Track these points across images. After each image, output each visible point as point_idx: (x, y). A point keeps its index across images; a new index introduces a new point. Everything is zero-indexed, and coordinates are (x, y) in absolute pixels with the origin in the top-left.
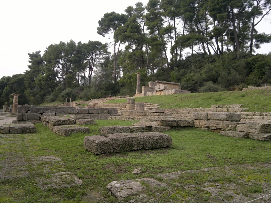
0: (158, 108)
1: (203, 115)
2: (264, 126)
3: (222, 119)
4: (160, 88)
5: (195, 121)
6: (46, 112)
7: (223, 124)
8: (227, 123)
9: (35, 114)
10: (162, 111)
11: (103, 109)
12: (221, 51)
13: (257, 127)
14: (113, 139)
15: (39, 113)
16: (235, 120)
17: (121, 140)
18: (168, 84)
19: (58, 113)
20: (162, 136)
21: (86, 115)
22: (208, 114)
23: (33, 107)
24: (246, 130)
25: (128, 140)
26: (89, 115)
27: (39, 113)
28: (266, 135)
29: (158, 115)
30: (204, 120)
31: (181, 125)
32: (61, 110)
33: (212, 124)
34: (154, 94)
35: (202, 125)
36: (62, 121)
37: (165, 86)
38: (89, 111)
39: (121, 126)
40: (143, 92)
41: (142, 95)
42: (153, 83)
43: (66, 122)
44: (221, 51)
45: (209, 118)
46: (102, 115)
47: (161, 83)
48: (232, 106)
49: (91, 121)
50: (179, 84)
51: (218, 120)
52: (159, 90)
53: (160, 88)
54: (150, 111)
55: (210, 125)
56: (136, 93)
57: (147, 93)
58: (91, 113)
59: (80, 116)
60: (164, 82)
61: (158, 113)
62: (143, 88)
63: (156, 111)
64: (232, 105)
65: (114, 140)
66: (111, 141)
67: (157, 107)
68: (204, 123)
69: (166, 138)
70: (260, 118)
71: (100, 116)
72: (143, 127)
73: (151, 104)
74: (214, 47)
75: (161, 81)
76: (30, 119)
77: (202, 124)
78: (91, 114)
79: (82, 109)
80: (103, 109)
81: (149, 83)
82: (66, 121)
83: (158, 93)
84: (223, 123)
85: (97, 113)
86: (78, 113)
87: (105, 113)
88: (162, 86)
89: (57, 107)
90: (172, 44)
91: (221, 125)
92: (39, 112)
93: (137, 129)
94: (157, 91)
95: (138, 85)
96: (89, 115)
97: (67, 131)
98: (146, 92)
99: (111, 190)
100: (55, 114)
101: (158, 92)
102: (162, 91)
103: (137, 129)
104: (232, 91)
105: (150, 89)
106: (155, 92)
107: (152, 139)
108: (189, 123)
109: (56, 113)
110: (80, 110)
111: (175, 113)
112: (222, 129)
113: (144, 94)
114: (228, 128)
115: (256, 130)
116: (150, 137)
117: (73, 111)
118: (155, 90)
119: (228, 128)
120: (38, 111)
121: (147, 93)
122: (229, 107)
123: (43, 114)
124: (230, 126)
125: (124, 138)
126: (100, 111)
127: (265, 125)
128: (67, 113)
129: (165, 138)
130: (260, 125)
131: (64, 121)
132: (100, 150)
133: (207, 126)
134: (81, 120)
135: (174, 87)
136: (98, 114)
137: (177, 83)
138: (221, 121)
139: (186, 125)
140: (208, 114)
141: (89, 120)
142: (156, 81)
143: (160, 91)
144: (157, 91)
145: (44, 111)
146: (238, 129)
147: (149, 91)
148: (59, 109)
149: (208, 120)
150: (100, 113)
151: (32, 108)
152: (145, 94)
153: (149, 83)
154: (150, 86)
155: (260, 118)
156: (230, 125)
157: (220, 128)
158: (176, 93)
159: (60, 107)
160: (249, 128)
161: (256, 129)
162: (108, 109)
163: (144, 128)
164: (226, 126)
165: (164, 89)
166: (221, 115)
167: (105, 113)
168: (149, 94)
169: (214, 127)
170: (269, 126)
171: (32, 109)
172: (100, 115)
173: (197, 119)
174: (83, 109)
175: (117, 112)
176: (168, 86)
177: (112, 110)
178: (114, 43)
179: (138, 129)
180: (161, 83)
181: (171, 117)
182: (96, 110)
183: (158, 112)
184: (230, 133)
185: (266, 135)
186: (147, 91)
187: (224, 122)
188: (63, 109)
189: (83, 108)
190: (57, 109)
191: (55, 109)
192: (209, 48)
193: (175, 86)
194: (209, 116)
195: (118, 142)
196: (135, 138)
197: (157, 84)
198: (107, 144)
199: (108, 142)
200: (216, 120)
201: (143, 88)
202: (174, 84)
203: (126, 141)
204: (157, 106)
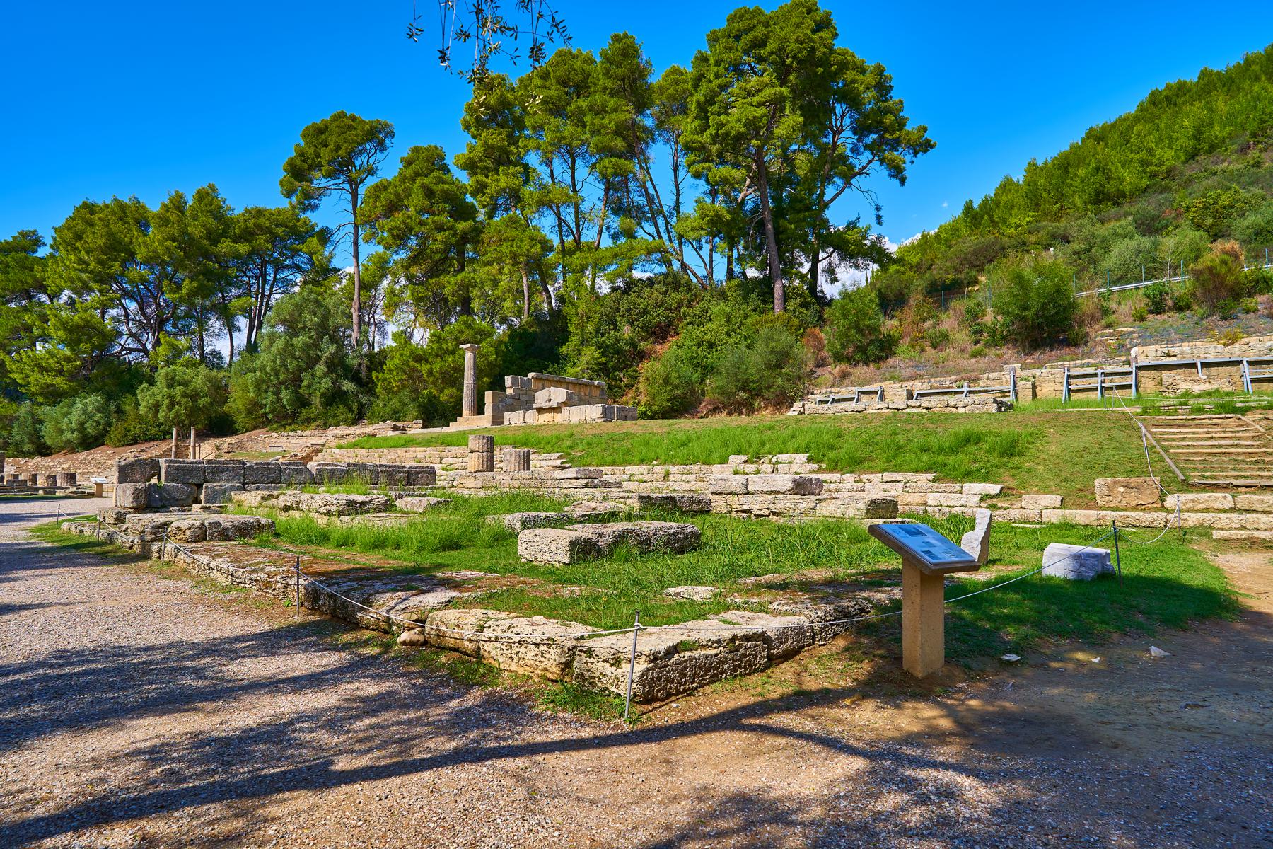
1: (735, 483)
4: (550, 400)
10: (592, 475)
12: (1167, 654)
29: (586, 486)
34: (532, 418)
40: (489, 409)
44: (1167, 654)
45: (750, 488)
48: (783, 457)
51: (772, 492)
52: (548, 405)
53: (552, 398)
55: (754, 507)
56: (461, 415)
57: (507, 415)
61: (585, 481)
63: (577, 472)
83: (546, 418)
91: (780, 506)
94: (540, 410)
115: (859, 513)
118: (534, 406)
121: (507, 415)
122: (778, 463)
124: (803, 505)
130: (866, 501)
133: (745, 507)
144: (540, 410)
154: (510, 392)
165: (565, 404)
168: (513, 418)
173: (721, 493)
178: (351, 228)
187: (789, 497)
190: (249, 468)
200: (766, 492)
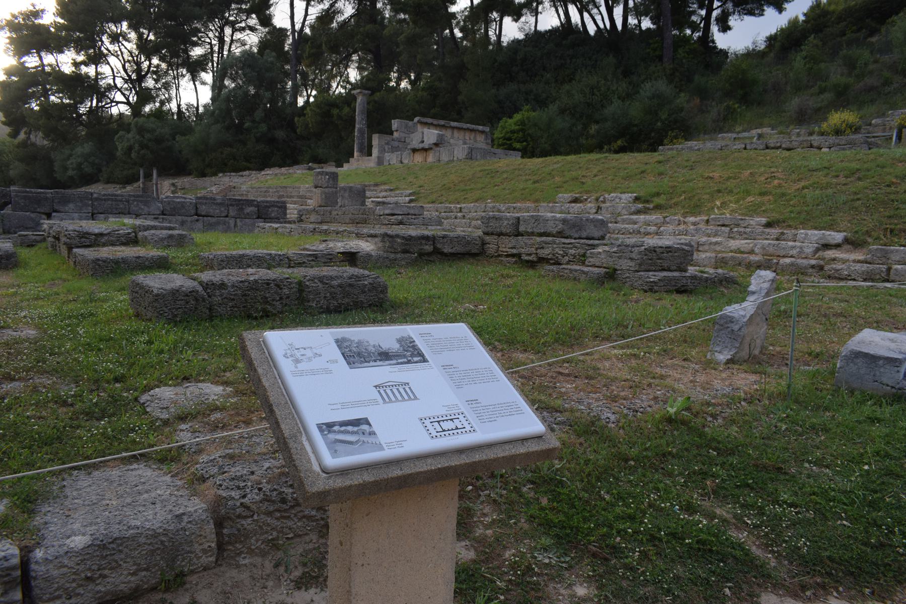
0: (411, 201)
2: (655, 251)
3: (554, 231)
5: (487, 238)
6: (62, 210)
7: (555, 246)
8: (564, 243)
9: (28, 213)
10: (412, 212)
11: (242, 202)
13: (634, 256)
14: (207, 284)
15: (39, 213)
16: (591, 235)
17: (233, 286)
18: (453, 128)
19: (100, 211)
20: (358, 278)
21: (189, 219)
22: (521, 218)
23: (19, 192)
24: (610, 262)
25: (254, 286)
26: (197, 220)
27: (39, 213)
28: (654, 276)
30: (510, 236)
31: (445, 251)
32: (109, 202)
33: (526, 246)
35: (504, 250)
36: (95, 235)
37: (439, 136)
38: (197, 208)
39: (260, 251)
40: (375, 152)
41: (370, 163)
42: (406, 126)
43: (106, 238)
45: (522, 228)
46: (238, 220)
47: (432, 124)
49: (179, 235)
50: (487, 129)
53: (425, 139)
54: (379, 210)
57: (387, 156)
58: (203, 213)
59: (170, 222)
60: (442, 122)
61: (400, 217)
62: (376, 140)
64: (612, 195)
65: (206, 286)
66: (200, 289)
67: (407, 199)
68: (507, 245)
69: (370, 284)
70: (677, 232)
71: (232, 225)
72: (331, 254)
73: (391, 190)
74: (598, 18)
75: (429, 120)
76: (12, 231)
77: (503, 246)
78: (204, 216)
79: (174, 201)
80: (242, 202)
81: (395, 124)
82: (106, 235)
84: (555, 243)
85: (224, 215)
86: (165, 215)
87: (248, 214)
88: (430, 135)
89: (95, 195)
90: (308, 18)
92: (38, 210)
93: (310, 259)
94: (414, 151)
95: (360, 130)
96: (197, 220)
97: (100, 262)
98: (382, 151)
99: (274, 440)
100: (92, 215)
101: (419, 153)
102: (431, 149)
103: (310, 259)
104: (544, 154)
105: (396, 144)
106: (410, 151)
107: (327, 284)
108: (468, 243)
109: (95, 211)
110: (169, 203)
111: (456, 218)
112: (551, 262)
113: (378, 157)
114: (567, 258)
116: (321, 279)
117: (146, 209)
119: (567, 258)
120: (36, 206)
123: (54, 214)
125: (241, 282)
126: (231, 207)
127: (657, 250)
128: (129, 214)
129: (366, 283)
131: (101, 235)
132: (166, 314)
133: (514, 251)
134: (153, 232)
135: (472, 138)
136: (227, 216)
137: (480, 128)
138: (550, 239)
139: (458, 249)
140: (518, 218)
141: (176, 232)
142: (416, 119)
143: (425, 150)
144: (414, 151)
145: (56, 207)
146: (591, 260)
147: (394, 149)
148: (102, 200)
149: (518, 234)
150: (232, 213)
151: (17, 196)
152: (380, 162)
153: (395, 124)
155: (677, 232)
156: (571, 248)
157: (547, 259)
158: (470, 156)
159: (104, 195)
160: (616, 257)
161: (631, 259)
162: (255, 203)
163: (330, 257)
164: (561, 252)
165: (436, 145)
166: (552, 222)
167: (248, 216)
169: (533, 256)
170: (668, 252)
171: (16, 199)
172: (232, 222)
174: (178, 200)
175: (285, 214)
176: (453, 133)
177: (266, 206)
179: (313, 260)
180: (432, 124)
181: (439, 227)
182: (221, 204)
183: (401, 213)
184: (566, 271)
185: (654, 276)
186: (387, 149)
188: (116, 200)
189: (178, 197)
190: (97, 199)
191: (91, 199)
192: (585, 20)
193: (473, 134)
194: (521, 222)
195: (223, 291)
196: (273, 281)
197: (419, 126)
198: (187, 295)
199: (190, 292)
201: (376, 140)
202: (472, 130)
203: (248, 290)
204: (410, 195)
